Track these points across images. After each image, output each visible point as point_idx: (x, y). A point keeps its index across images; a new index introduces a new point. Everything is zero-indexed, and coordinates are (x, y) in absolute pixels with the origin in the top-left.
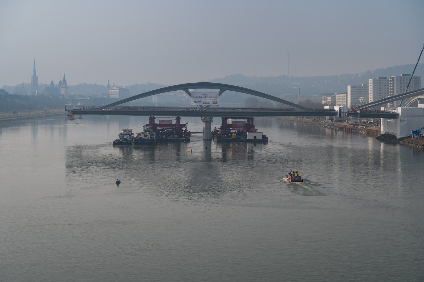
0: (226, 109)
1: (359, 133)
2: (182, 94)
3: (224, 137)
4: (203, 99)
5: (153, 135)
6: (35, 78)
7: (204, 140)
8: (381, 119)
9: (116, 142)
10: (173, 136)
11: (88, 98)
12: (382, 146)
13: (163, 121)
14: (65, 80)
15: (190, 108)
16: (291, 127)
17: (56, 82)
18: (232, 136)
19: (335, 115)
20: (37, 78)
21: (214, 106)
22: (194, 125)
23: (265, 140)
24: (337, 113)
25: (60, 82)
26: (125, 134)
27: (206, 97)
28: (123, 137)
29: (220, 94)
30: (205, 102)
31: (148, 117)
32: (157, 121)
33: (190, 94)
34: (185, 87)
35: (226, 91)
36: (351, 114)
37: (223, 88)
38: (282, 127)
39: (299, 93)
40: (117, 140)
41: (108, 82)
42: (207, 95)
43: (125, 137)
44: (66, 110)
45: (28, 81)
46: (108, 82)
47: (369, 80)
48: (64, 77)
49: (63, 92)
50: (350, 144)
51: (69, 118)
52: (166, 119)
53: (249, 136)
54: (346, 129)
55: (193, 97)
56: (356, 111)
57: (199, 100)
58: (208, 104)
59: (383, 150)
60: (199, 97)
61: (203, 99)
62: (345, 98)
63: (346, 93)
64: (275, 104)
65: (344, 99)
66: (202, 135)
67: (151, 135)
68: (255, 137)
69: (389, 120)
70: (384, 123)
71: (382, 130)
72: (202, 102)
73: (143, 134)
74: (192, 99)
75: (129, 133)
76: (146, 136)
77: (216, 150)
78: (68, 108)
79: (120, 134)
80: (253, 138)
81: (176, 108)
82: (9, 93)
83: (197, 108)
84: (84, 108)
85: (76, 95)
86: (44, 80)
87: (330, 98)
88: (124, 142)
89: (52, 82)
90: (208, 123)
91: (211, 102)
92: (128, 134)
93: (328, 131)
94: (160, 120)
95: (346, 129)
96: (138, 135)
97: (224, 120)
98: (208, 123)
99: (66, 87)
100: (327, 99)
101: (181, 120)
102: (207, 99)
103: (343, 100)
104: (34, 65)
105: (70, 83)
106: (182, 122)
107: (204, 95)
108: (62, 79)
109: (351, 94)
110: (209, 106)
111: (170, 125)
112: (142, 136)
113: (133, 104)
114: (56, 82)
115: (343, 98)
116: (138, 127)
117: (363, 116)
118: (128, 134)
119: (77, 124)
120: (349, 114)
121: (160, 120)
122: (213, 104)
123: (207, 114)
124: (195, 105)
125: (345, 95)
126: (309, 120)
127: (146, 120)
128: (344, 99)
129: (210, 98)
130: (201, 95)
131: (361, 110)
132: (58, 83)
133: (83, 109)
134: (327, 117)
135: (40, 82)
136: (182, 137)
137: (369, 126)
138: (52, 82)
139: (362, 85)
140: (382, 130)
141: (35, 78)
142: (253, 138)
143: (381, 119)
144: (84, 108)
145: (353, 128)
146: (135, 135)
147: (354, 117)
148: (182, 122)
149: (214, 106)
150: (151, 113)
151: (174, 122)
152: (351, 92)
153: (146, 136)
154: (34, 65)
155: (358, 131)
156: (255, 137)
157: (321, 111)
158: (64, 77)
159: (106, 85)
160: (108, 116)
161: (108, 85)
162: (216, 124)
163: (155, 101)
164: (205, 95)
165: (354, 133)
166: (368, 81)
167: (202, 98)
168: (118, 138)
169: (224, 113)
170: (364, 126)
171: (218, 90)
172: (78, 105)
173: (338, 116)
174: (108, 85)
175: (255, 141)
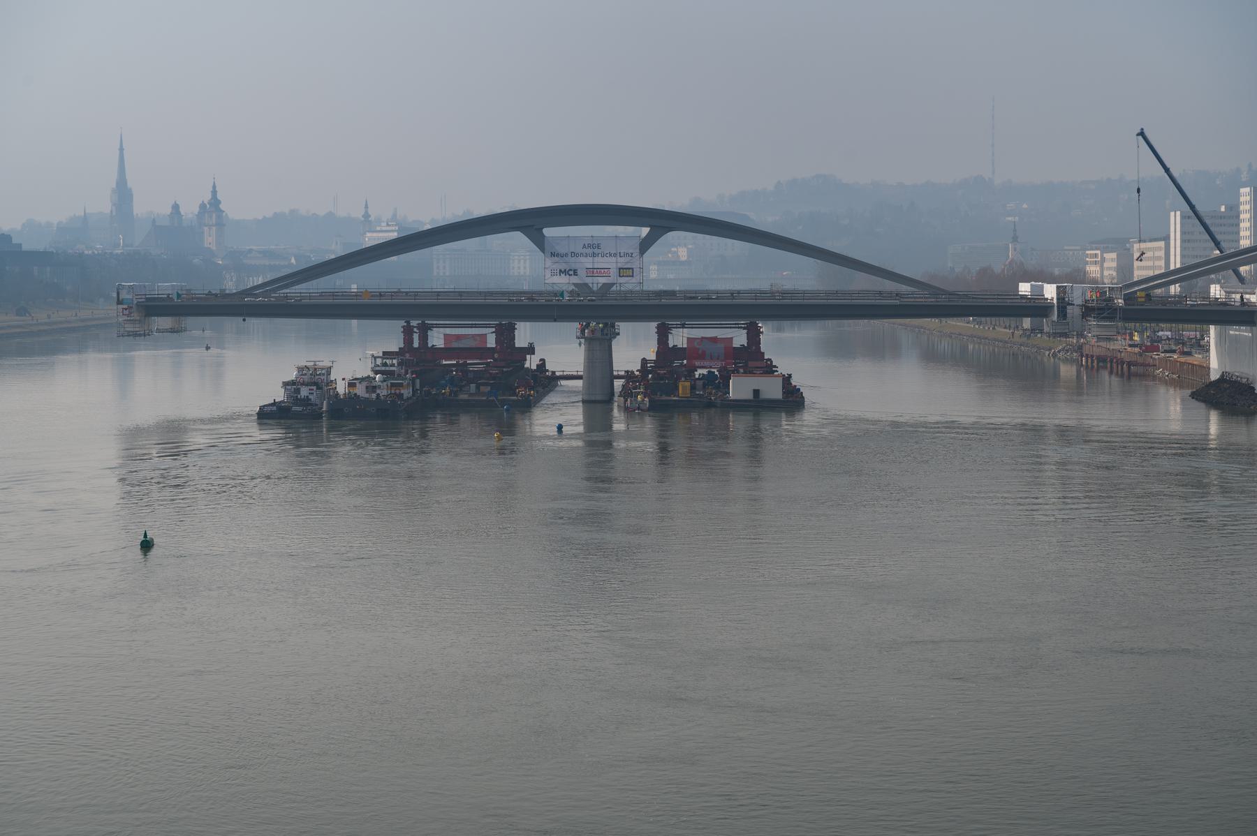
0: (672, 294)
1: (1154, 378)
2: (517, 240)
3: (673, 393)
4: (588, 262)
5: (401, 385)
6: (123, 194)
7: (584, 402)
8: (1212, 328)
9: (269, 409)
10: (478, 388)
11: (293, 261)
12: (1214, 425)
13: (458, 337)
14: (215, 202)
15: (540, 293)
16: (960, 360)
17: (190, 209)
18: (677, 388)
19: (1046, 316)
20: (131, 195)
21: (629, 284)
22: (559, 349)
23: (792, 400)
24: (1050, 307)
25: (203, 206)
26: (303, 384)
27: (594, 255)
28: (298, 391)
29: (645, 245)
30: (592, 272)
31: (653, 326)
32: (437, 339)
33: (540, 241)
34: (530, 222)
35: (671, 234)
36: (1093, 309)
37: (661, 222)
38: (931, 357)
39: (1015, 239)
40: (274, 404)
41: (366, 207)
42: (598, 247)
43: (304, 392)
44: (119, 302)
45: (102, 204)
46: (366, 207)
47: (1242, 190)
48: (214, 192)
49: (210, 240)
50: (1106, 414)
51: (129, 328)
52: (468, 331)
53: (739, 388)
54: (1111, 362)
55: (553, 255)
56: (1111, 299)
57: (573, 266)
58: (602, 280)
59: (1219, 437)
60: (574, 254)
61: (588, 262)
62: (1162, 253)
63: (1166, 239)
64: (861, 283)
65: (1159, 258)
66: (579, 383)
67: (392, 385)
68: (756, 392)
69: (1233, 331)
70: (1221, 338)
71: (1215, 365)
72: (582, 273)
73: (365, 384)
74: (549, 262)
75: (316, 378)
76: (372, 389)
77: (634, 438)
78: (125, 295)
79: (286, 384)
80: (750, 396)
81: (491, 293)
82: (25, 247)
83: (562, 294)
84: (179, 296)
85: (250, 251)
86: (151, 203)
87: (1114, 255)
88: (305, 414)
89: (176, 207)
90: (599, 347)
91: (614, 272)
92: (315, 384)
93: (1067, 371)
94: (445, 335)
95: (1111, 362)
96: (351, 385)
97: (663, 333)
98: (599, 347)
99: (221, 223)
100: (1103, 260)
101: (516, 332)
102: (601, 262)
103: (1157, 263)
104: (121, 149)
105: (233, 209)
106: (521, 341)
107: (590, 246)
108: (207, 197)
109: (1183, 241)
110: (613, 284)
111: (482, 352)
112: (360, 390)
113: (353, 282)
114: (190, 209)
115: (1157, 254)
116: (353, 358)
117: (1143, 323)
118: (315, 384)
119: (208, 348)
120: (1087, 311)
121: (445, 335)
122: (622, 280)
123: (597, 314)
124: (563, 282)
125: (1162, 244)
126: (1000, 329)
127: (387, 338)
128: (1159, 258)
129: (605, 257)
130: (579, 250)
131: (1128, 298)
132: (196, 210)
133: (175, 297)
134: (1027, 323)
135: (141, 207)
136: (511, 388)
137: (1189, 354)
138: (176, 207)
139: (1223, 209)
140: (1215, 365)
141: (123, 194)
142: (750, 396)
143: (1212, 328)
144: (179, 296)
145: (1140, 360)
146: (341, 388)
147: (1104, 319)
148: (521, 341)
149: (630, 287)
150: (414, 310)
151: (740, 338)
152: (1183, 233)
153: (372, 389)
154: (121, 149)
155: (1151, 369)
156: (756, 392)
157: (1009, 302)
158: (214, 192)
159: (358, 214)
160: (354, 322)
161: (367, 216)
162: (633, 349)
163: (445, 269)
164: (594, 247)
165: (1137, 375)
166: (1238, 195)
167: (582, 259)
168: (280, 395)
169: (663, 309)
170: (1174, 351)
171: (645, 231)
172: (165, 287)
173: (1055, 318)
174: (367, 216)
175: (757, 405)
